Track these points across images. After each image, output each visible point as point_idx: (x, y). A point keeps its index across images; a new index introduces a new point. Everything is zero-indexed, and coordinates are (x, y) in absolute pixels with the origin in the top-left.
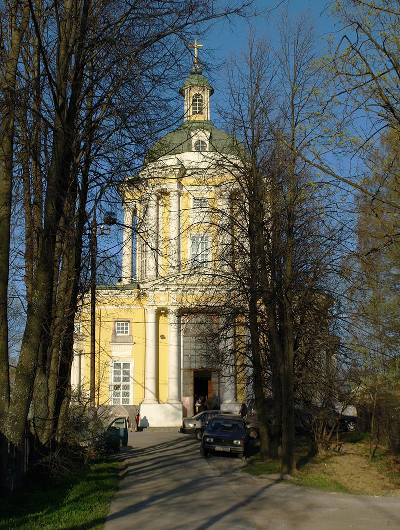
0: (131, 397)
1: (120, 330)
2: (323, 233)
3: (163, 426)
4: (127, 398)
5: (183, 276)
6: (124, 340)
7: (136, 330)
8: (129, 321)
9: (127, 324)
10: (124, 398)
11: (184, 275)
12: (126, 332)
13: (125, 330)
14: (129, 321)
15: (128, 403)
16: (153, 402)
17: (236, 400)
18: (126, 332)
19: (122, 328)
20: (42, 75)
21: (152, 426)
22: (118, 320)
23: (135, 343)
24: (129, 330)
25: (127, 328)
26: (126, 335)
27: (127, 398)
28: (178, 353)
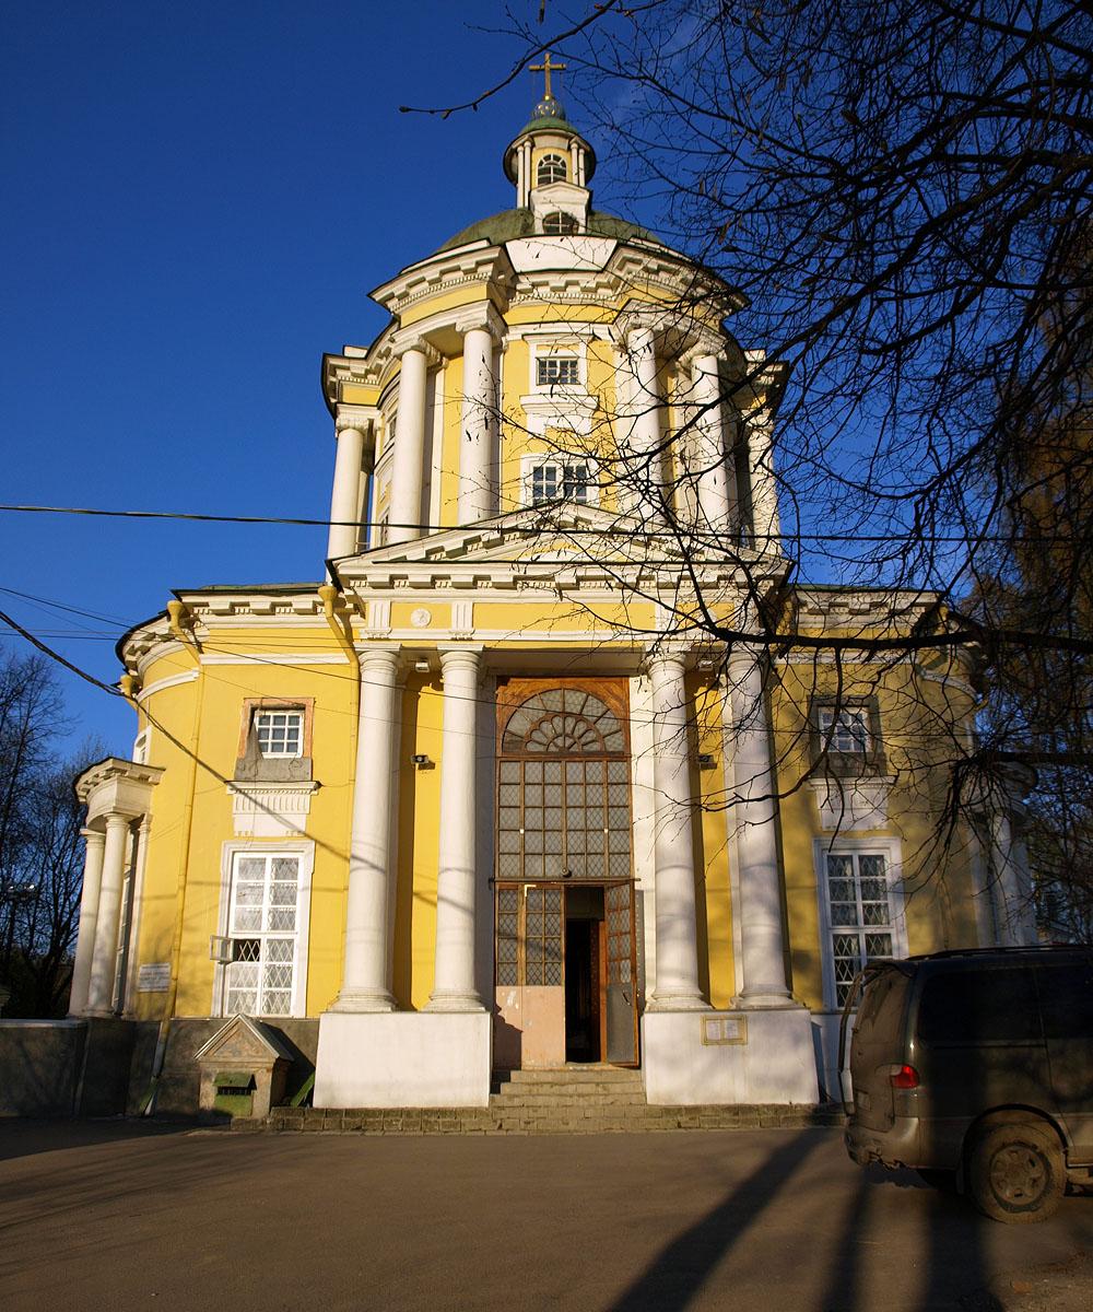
0: (297, 989)
1: (286, 741)
2: (1065, 452)
3: (410, 1105)
4: (283, 990)
5: (496, 535)
6: (278, 775)
7: (323, 735)
8: (301, 708)
9: (294, 720)
10: (274, 989)
11: (503, 531)
12: (292, 747)
13: (286, 741)
14: (301, 708)
15: (287, 1012)
16: (466, 1005)
17: (706, 997)
18: (292, 747)
19: (278, 733)
20: (675, 531)
21: (348, 1099)
22: (265, 703)
23: (319, 785)
24: (300, 741)
25: (294, 733)
26: (291, 755)
27: (283, 990)
28: (779, 880)
